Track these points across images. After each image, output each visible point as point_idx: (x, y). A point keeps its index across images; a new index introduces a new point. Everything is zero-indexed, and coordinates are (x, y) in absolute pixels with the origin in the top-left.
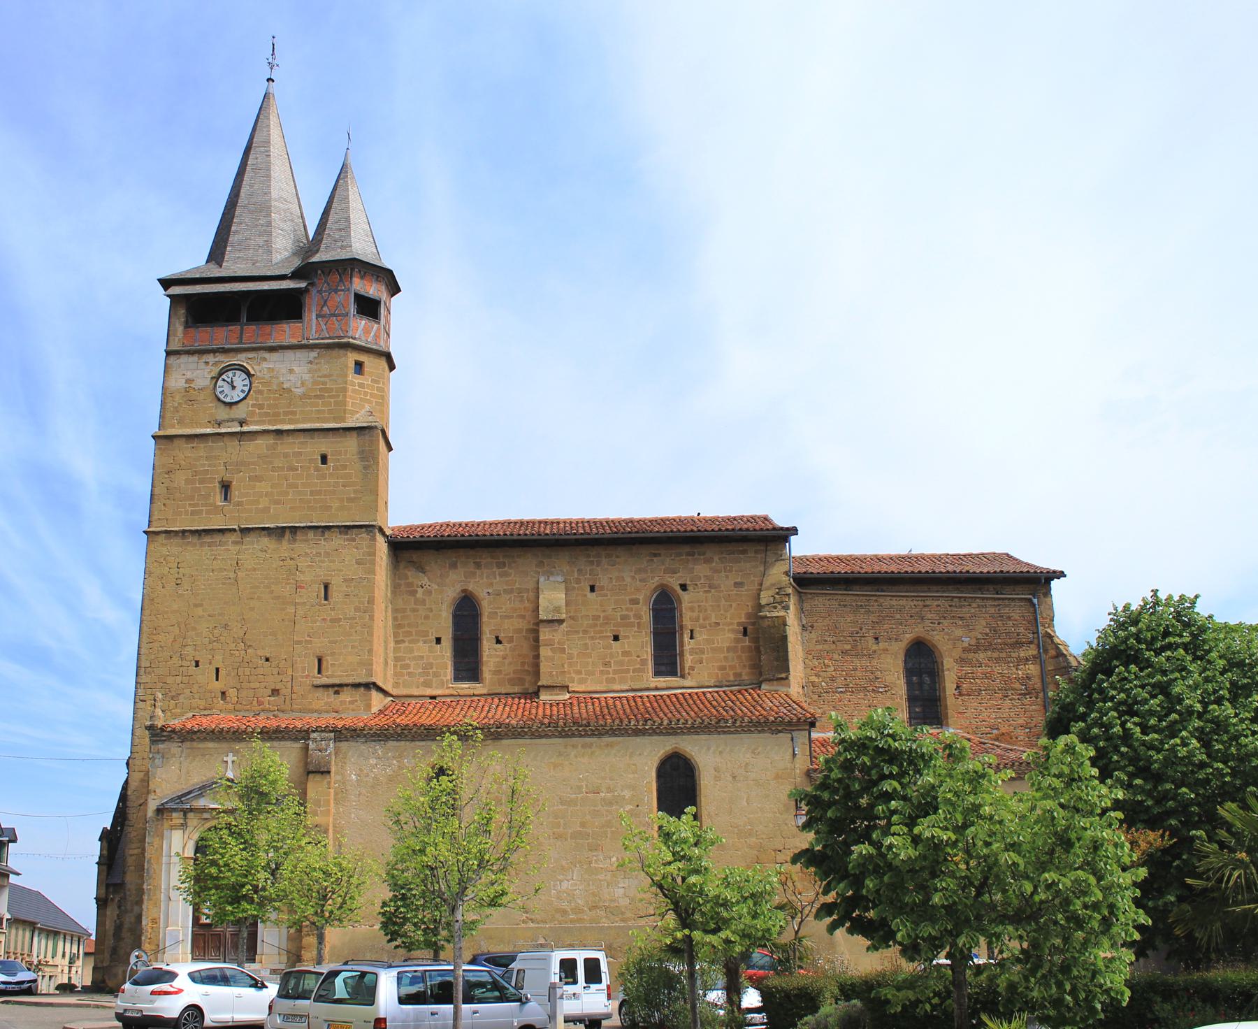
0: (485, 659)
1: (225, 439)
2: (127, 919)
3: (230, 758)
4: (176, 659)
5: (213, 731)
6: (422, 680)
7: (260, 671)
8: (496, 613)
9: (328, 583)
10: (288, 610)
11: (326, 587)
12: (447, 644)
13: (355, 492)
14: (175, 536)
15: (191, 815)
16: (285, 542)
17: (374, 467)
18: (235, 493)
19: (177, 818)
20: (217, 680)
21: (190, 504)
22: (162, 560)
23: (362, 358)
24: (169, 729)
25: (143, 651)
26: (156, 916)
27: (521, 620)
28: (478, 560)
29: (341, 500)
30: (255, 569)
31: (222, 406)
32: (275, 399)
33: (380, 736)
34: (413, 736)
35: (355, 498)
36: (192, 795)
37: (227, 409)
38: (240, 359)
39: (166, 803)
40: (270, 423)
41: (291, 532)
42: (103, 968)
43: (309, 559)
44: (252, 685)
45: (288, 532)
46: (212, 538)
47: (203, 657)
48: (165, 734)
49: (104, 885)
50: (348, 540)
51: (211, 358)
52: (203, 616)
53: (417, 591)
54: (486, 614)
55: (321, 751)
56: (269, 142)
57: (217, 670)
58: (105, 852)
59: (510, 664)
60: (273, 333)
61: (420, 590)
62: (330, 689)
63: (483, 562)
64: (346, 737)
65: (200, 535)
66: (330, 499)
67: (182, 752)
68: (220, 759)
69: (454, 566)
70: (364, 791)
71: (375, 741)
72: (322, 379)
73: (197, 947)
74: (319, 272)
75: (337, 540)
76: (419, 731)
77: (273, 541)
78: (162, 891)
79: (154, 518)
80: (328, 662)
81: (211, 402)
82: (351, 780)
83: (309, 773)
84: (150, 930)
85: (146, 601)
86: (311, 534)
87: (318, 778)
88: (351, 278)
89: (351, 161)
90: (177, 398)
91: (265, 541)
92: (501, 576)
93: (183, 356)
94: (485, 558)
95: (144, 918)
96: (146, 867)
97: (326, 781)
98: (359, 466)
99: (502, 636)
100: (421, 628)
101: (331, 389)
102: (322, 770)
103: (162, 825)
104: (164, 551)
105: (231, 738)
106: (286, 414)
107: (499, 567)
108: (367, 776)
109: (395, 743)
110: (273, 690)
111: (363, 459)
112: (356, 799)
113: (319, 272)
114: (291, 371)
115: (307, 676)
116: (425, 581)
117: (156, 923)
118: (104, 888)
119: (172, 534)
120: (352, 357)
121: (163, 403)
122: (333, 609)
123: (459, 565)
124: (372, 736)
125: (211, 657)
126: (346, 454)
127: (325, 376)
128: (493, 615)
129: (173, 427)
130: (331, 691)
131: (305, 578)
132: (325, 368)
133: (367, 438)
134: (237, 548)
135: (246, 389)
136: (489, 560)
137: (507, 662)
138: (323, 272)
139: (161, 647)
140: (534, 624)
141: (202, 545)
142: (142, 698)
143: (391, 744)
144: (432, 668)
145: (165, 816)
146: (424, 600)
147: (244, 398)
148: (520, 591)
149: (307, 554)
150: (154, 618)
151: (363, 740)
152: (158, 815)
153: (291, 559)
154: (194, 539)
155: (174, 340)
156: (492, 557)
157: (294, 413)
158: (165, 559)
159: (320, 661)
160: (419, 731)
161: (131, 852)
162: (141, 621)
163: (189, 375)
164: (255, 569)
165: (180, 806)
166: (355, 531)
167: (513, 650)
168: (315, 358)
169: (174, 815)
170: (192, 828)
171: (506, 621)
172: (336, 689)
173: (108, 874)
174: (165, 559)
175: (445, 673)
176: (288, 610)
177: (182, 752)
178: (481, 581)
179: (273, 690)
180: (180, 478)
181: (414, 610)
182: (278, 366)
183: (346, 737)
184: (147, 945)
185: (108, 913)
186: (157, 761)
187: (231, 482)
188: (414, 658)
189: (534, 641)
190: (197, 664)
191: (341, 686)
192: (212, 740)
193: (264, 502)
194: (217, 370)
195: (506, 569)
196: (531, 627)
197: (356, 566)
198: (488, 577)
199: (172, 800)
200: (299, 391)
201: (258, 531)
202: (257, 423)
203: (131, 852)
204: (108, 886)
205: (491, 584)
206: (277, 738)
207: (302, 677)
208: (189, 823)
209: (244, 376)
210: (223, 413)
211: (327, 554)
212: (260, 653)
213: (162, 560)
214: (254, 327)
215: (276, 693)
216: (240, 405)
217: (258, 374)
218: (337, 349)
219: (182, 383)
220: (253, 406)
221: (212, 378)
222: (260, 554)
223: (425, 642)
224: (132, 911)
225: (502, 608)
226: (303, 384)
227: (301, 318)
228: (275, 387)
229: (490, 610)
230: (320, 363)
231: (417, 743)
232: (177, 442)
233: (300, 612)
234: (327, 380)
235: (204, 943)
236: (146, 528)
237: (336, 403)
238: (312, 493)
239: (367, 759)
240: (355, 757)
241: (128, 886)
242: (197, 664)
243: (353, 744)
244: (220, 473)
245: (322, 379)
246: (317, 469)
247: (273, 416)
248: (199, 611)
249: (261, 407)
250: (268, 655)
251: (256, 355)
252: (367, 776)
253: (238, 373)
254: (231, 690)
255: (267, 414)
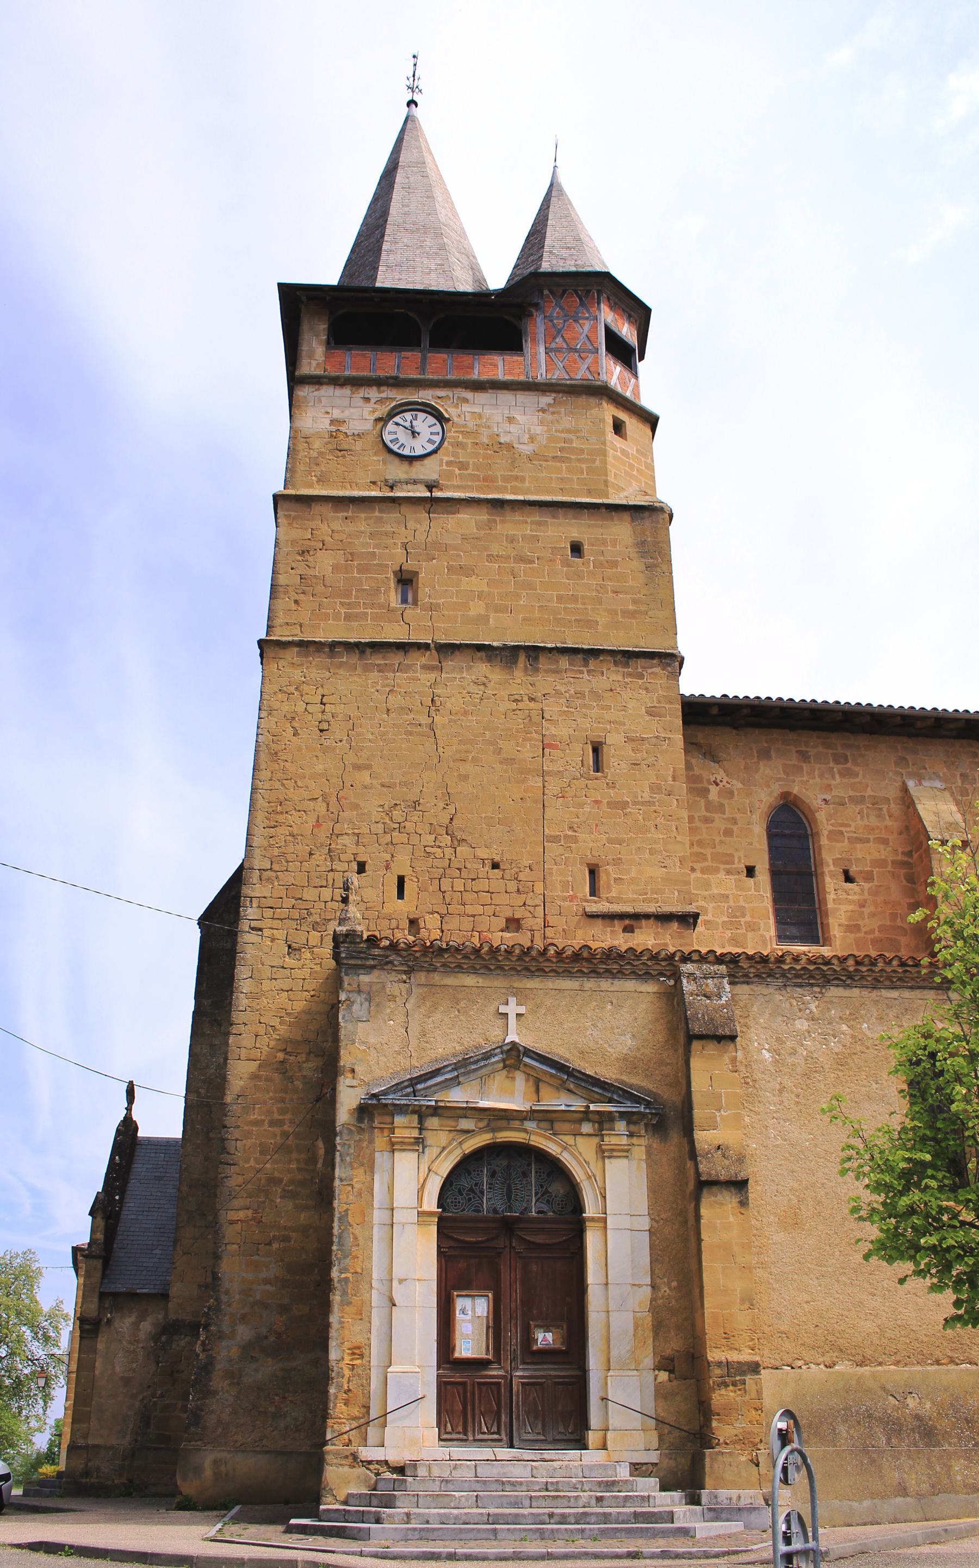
0: (830, 905)
1: (405, 509)
2: (224, 1353)
3: (512, 1008)
4: (320, 858)
5: (477, 951)
6: (728, 934)
7: (483, 885)
8: (842, 833)
9: (601, 743)
10: (531, 783)
11: (597, 750)
12: (763, 877)
13: (635, 602)
14: (318, 651)
15: (432, 1122)
16: (519, 673)
17: (665, 567)
18: (424, 592)
19: (404, 1126)
20: (401, 895)
21: (341, 603)
22: (292, 689)
23: (623, 416)
24: (386, 943)
25: (256, 842)
26: (359, 1339)
27: (882, 847)
28: (803, 749)
29: (613, 613)
30: (465, 713)
31: (396, 461)
32: (486, 457)
33: (812, 977)
34: (876, 979)
35: (635, 611)
36: (439, 1079)
37: (405, 466)
38: (426, 396)
39: (385, 1093)
40: (479, 489)
41: (528, 657)
42: (87, 1447)
43: (563, 701)
44: (470, 910)
45: (522, 658)
46: (384, 658)
47: (374, 855)
48: (376, 952)
49: (97, 1294)
50: (630, 675)
51: (373, 393)
52: (371, 787)
53: (708, 790)
54: (825, 833)
55: (708, 997)
56: (424, 163)
57: (401, 881)
58: (100, 1236)
59: (873, 915)
60: (477, 365)
61: (713, 788)
62: (616, 922)
63: (812, 752)
64: (746, 975)
65: (362, 652)
66: (593, 609)
67: (410, 992)
68: (492, 1009)
69: (765, 754)
70: (788, 1083)
71: (801, 986)
72: (563, 435)
73: (450, 1413)
74: (546, 292)
75: (611, 676)
76: (889, 969)
77: (497, 669)
78: (375, 1284)
79: (278, 621)
80: (608, 874)
81: (376, 454)
82: (763, 1061)
83: (691, 1037)
84: (347, 1373)
85: (263, 757)
86: (564, 662)
87: (711, 1048)
88: (599, 303)
89: (563, 180)
90: (317, 444)
91: (482, 668)
92: (842, 775)
93: (325, 387)
94: (814, 744)
95: (332, 1344)
96: (336, 1231)
97: (726, 1058)
98: (637, 564)
99: (853, 870)
100: (719, 849)
101: (582, 450)
102: (720, 1032)
103: (371, 1141)
104: (297, 674)
105: (513, 969)
106: (506, 479)
107: (837, 761)
108: (794, 1052)
109: (841, 992)
110: (508, 920)
111: (643, 554)
112: (776, 1099)
113: (546, 292)
114: (511, 420)
115: (572, 898)
116: (720, 775)
117: (362, 1356)
118: (96, 1300)
119: (312, 649)
120: (609, 412)
121: (292, 452)
122: (613, 785)
123: (773, 754)
124: (797, 976)
125: (388, 857)
126: (614, 545)
127: (569, 431)
128: (836, 835)
129: (311, 486)
130: (618, 925)
131: (560, 731)
132: (567, 422)
133: (647, 523)
134: (432, 676)
135: (437, 439)
136: (821, 749)
137: (866, 911)
138: (552, 292)
139: (292, 835)
140: (903, 853)
141: (367, 669)
142: (254, 924)
143: (834, 992)
144: (744, 915)
145: (376, 1124)
146: (722, 805)
147: (434, 452)
148: (875, 802)
149: (558, 693)
150: (277, 785)
151: (780, 982)
152: (360, 1119)
153: (532, 699)
154: (354, 659)
155: (310, 363)
156: (828, 746)
157: (522, 479)
158: (297, 689)
159: (593, 872)
160: (889, 969)
161: (232, 1215)
162: (254, 790)
163: (336, 414)
164: (465, 713)
165: (411, 1101)
166: (641, 662)
167: (874, 893)
168: (549, 405)
169: (399, 1120)
170: (436, 1151)
171: (858, 846)
172: (627, 922)
173: (104, 1276)
174: (297, 689)
175: (767, 924)
176: (531, 783)
177: (410, 992)
178: (811, 781)
179: (508, 920)
180: (324, 563)
181: (707, 820)
182: (488, 411)
183: (746, 975)
184: (341, 1406)
185: (101, 1346)
186: (356, 1007)
187: (416, 573)
188: (713, 898)
189: (908, 881)
190: (361, 868)
191: (637, 917)
192: (474, 971)
193: (477, 608)
194: (383, 410)
195: (849, 765)
196: (899, 858)
197: (647, 718)
198: (821, 776)
199: (397, 1088)
200: (527, 449)
201: (469, 652)
202: (458, 488)
203: (232, 1215)
204: (103, 1296)
205: (828, 788)
206: (608, 971)
207: (564, 899)
208: (430, 1138)
209: (431, 420)
210: (397, 471)
211: (596, 695)
212: (482, 853)
213: (292, 689)
214: (445, 356)
215: (513, 926)
216: (427, 461)
217: (456, 419)
218: (584, 396)
219: (324, 424)
220: (449, 463)
221: (378, 420)
222: (474, 689)
223: (728, 872)
224: (233, 1333)
225: (850, 826)
226: (532, 439)
227: (522, 350)
228: (486, 440)
229: (831, 828)
230: (559, 413)
231: (885, 993)
232: (317, 509)
233: (554, 787)
234: (571, 436)
235: (499, 1404)
236: (263, 636)
237: (590, 471)
238: (560, 598)
239: (789, 1020)
240: (767, 1016)
241: (226, 1285)
242: (361, 868)
243: (759, 989)
244: (396, 558)
245: (563, 435)
246: (566, 564)
247: (485, 480)
248: (365, 777)
249: (463, 466)
250: (497, 859)
251: (451, 394)
252: (794, 1052)
253: (421, 416)
254: (428, 917)
255: (475, 478)
